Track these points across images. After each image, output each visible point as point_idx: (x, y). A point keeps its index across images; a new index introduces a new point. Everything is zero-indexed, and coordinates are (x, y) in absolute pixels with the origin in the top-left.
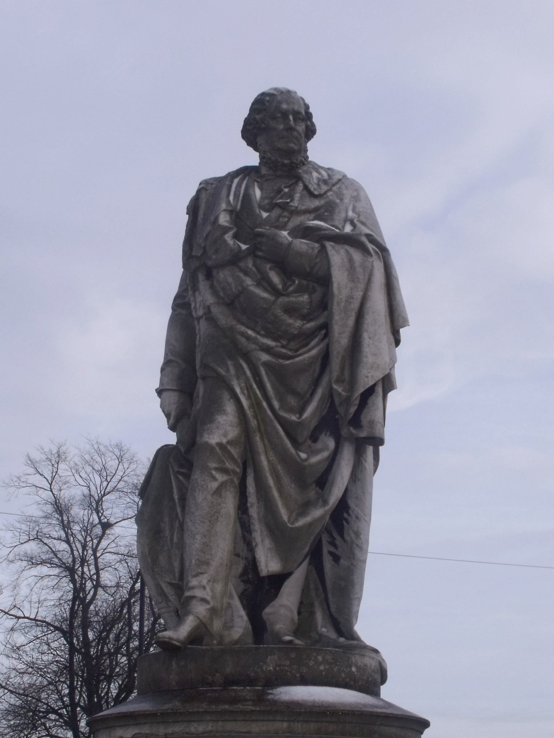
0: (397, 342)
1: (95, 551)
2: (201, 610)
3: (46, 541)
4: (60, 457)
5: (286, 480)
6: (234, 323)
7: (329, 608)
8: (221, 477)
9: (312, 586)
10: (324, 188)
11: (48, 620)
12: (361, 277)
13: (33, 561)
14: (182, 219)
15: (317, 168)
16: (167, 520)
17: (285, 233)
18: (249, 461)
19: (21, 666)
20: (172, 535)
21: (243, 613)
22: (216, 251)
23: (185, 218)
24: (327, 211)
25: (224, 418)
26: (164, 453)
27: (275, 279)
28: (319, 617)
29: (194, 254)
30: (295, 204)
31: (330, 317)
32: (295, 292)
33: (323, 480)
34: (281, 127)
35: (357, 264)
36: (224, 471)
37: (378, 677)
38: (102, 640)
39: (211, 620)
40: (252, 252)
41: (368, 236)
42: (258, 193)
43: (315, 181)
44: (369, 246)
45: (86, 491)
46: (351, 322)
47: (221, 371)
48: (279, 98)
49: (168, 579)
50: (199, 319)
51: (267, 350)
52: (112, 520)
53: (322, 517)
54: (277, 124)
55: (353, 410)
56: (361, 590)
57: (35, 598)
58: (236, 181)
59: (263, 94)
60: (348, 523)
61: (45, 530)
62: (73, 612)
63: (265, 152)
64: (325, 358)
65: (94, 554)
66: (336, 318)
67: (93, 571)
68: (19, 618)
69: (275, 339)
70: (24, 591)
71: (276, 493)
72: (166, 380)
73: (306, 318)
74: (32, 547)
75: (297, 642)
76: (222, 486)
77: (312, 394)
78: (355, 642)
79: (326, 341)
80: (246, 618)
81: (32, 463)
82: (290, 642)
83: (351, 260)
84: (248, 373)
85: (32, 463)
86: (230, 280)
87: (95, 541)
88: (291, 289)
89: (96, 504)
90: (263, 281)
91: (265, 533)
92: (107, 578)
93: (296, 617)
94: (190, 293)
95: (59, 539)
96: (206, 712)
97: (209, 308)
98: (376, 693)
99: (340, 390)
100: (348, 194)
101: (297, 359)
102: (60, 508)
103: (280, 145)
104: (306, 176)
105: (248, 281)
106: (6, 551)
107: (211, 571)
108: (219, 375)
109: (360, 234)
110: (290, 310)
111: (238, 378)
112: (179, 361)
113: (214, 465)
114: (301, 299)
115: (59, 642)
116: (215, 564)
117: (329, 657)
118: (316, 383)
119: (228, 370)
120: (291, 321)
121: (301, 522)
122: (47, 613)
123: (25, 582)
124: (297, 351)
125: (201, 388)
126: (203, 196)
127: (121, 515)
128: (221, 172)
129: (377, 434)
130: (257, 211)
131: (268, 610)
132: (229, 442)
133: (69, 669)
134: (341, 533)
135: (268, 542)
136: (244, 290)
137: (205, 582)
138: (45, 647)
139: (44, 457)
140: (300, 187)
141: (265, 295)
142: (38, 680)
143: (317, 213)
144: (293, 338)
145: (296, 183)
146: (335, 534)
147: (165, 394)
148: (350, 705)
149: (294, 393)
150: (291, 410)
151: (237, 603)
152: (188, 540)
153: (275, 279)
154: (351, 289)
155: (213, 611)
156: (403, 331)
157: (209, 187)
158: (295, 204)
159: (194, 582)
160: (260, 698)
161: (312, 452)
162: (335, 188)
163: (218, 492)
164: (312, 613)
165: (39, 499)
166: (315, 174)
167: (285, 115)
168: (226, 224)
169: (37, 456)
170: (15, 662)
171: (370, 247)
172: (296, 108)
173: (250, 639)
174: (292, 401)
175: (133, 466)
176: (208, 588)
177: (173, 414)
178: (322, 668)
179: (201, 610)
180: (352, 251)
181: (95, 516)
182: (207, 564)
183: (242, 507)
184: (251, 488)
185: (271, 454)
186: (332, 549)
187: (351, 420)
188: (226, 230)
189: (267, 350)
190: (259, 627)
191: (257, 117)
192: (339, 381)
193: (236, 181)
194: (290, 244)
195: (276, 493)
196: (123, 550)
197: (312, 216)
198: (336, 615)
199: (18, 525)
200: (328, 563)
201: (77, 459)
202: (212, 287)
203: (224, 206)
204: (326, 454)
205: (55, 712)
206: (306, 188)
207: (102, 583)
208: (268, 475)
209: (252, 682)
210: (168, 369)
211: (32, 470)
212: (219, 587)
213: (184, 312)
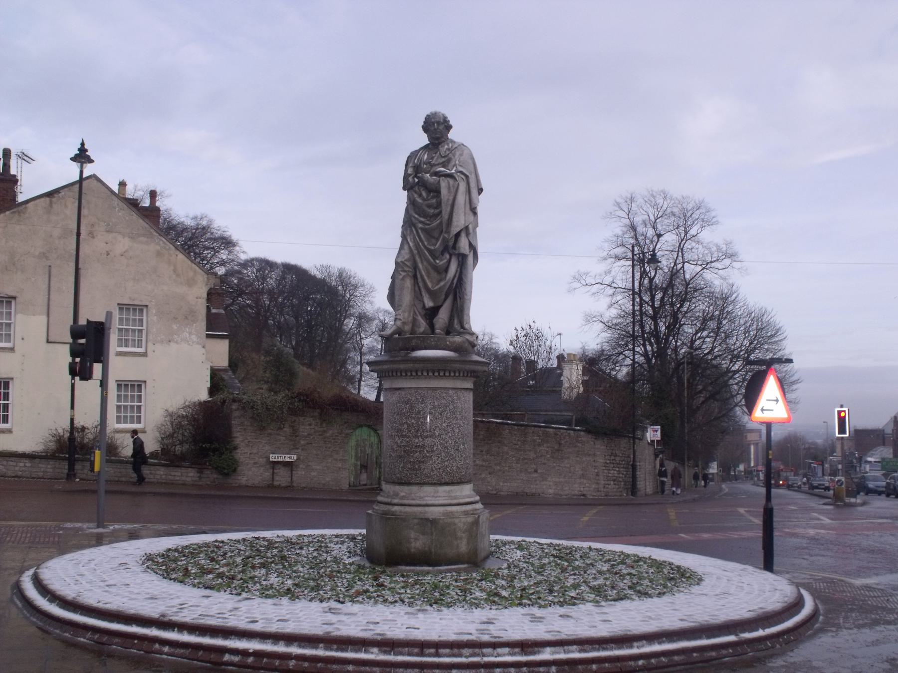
8: (403, 274)
13: (617, 258)
27: (424, 194)
28: (456, 321)
36: (404, 271)
51: (421, 222)
52: (662, 233)
81: (618, 205)
85: (618, 205)
105: (416, 196)
107: (403, 308)
110: (429, 206)
116: (404, 305)
128: (417, 148)
144: (431, 217)
149: (434, 237)
153: (424, 194)
161: (441, 260)
163: (403, 279)
169: (619, 200)
174: (434, 241)
189: (421, 222)
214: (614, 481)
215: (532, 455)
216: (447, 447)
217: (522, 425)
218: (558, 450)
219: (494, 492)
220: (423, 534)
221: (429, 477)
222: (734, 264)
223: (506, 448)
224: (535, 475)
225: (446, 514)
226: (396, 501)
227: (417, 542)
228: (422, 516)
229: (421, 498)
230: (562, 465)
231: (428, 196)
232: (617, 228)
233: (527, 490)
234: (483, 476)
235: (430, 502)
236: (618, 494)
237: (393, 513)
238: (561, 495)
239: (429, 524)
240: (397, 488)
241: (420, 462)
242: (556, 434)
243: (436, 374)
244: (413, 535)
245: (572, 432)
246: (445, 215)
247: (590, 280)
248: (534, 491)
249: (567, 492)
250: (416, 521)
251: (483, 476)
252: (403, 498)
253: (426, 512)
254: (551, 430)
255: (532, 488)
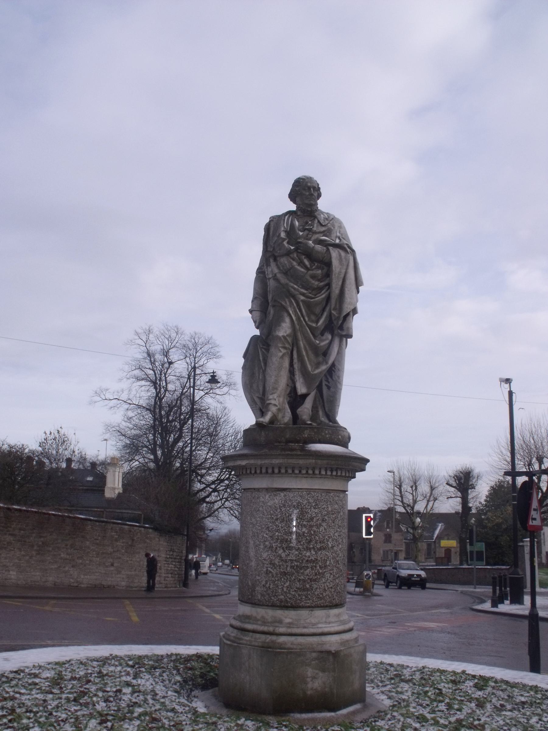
0: (358, 292)
1: (165, 374)
2: (274, 409)
3: (143, 369)
4: (150, 331)
5: (310, 352)
6: (288, 282)
7: (325, 409)
8: (283, 351)
9: (317, 399)
10: (327, 222)
11: (144, 405)
12: (345, 263)
13: (138, 379)
14: (262, 233)
15: (322, 213)
16: (257, 369)
17: (311, 242)
18: (295, 343)
19: (131, 426)
20: (259, 375)
21: (289, 411)
22: (280, 249)
23: (263, 233)
24: (328, 232)
25: (285, 324)
26: (254, 339)
27: (307, 262)
28: (321, 413)
29: (268, 250)
30: (315, 229)
31: (331, 280)
32: (315, 269)
33: (326, 353)
34: (307, 193)
35: (343, 258)
37: (348, 440)
38: (168, 415)
39: (278, 414)
40: (296, 250)
41: (347, 244)
42: (297, 223)
43: (323, 219)
44: (346, 248)
45: (162, 348)
46: (340, 283)
47: (283, 303)
48: (307, 180)
49: (257, 395)
50: (269, 279)
51: (303, 294)
52: (173, 361)
53: (324, 370)
54: (305, 192)
55: (340, 322)
56: (340, 401)
57: (138, 395)
58: (286, 217)
59: (299, 178)
60: (334, 371)
61: (143, 365)
62: (156, 403)
63: (300, 205)
64: (328, 298)
65: (165, 376)
66: (334, 281)
67: (164, 384)
68: (131, 404)
69: (306, 290)
70: (134, 392)
71: (306, 358)
72: (254, 306)
73: (320, 280)
74: (137, 372)
75: (314, 424)
76: (284, 355)
77: (322, 315)
78: (336, 425)
79: (329, 291)
80: (290, 413)
81: (137, 334)
82: (310, 424)
83: (340, 255)
84: (295, 304)
85: (137, 334)
86: (286, 262)
87: (165, 370)
88: (314, 267)
89: (166, 353)
90: (301, 263)
91: (300, 376)
92: (171, 387)
93: (311, 413)
94: (265, 267)
95: (149, 369)
96: (280, 455)
97: (275, 275)
98: (347, 447)
99: (335, 313)
100: (336, 225)
101: (316, 299)
102: (149, 355)
103: (307, 202)
104: (318, 216)
105: (295, 263)
106: (125, 374)
107: (278, 392)
108: (282, 305)
109: (343, 244)
110: (313, 277)
111: (291, 307)
112: (260, 298)
113: (280, 345)
114: (318, 272)
115: (149, 416)
117: (330, 431)
118: (323, 310)
119: (286, 303)
120: (313, 282)
121: (316, 372)
122: (143, 403)
123: (135, 388)
124: (315, 295)
125: (271, 311)
126: (272, 224)
127: (177, 358)
128: (280, 213)
129: (350, 334)
130: (297, 231)
131: (299, 410)
132: (287, 335)
133: (153, 427)
134: (331, 377)
135: (301, 380)
136: (293, 267)
137: (275, 397)
138: (142, 418)
139: (142, 331)
140: (316, 221)
141: (302, 270)
142: (137, 432)
143: (324, 233)
144: (314, 289)
145: (314, 219)
146: (328, 377)
147: (254, 312)
148: (340, 453)
149: (314, 314)
150: (312, 321)
151: (287, 406)
152: (268, 378)
153: (307, 262)
154: (340, 268)
155: (279, 410)
156: (361, 288)
157: (274, 220)
158: (315, 229)
159: (271, 397)
160: (303, 449)
161: (322, 341)
162: (331, 222)
163: (282, 357)
164: (318, 411)
165: (140, 350)
166: (322, 216)
167: (309, 188)
168: (284, 237)
169: (140, 331)
170: (128, 424)
171: (348, 250)
172: (314, 185)
173: (291, 422)
174: (313, 318)
175: (183, 336)
176: (277, 400)
177: (258, 321)
178: (327, 436)
179: (274, 409)
180: (341, 251)
181: (166, 359)
182: (277, 389)
183: (291, 364)
184: (295, 356)
185: (304, 341)
186: (327, 383)
187: (337, 325)
188: (284, 240)
189: (303, 294)
190: (295, 418)
191: (297, 189)
192: (335, 309)
193: (286, 217)
194: (314, 247)
195: (306, 358)
196: (178, 374)
197: (322, 235)
198: (328, 413)
199: (131, 362)
200: (325, 389)
201: (157, 333)
202: (277, 265)
203: (283, 229)
204: (327, 342)
205: (146, 447)
206: (319, 221)
207: (169, 389)
208: (303, 350)
209: (298, 442)
210: (255, 301)
211: (137, 337)
212: (281, 399)
213: (262, 275)
214: (171, 574)
215: (110, 550)
216: (338, 561)
217: (103, 522)
218: (131, 546)
219: (76, 584)
220: (323, 671)
221: (321, 599)
222: (232, 392)
223: (88, 543)
224: (112, 568)
225: (343, 643)
226: (282, 630)
227: (316, 682)
228: (319, 648)
229: (314, 625)
230: (134, 559)
231: (311, 266)
232: (138, 354)
233: (104, 583)
234: (67, 569)
235: (326, 630)
236: (174, 586)
237: (281, 646)
238: (132, 587)
239: (331, 657)
240: (279, 613)
241: (311, 580)
242: (130, 531)
243: (334, 473)
244: (310, 672)
245: (143, 529)
246: (336, 289)
247: (109, 396)
248: (110, 583)
249: (136, 585)
250: (314, 655)
251: (67, 569)
252: (290, 625)
253: (323, 644)
254: (126, 527)
255: (109, 581)
